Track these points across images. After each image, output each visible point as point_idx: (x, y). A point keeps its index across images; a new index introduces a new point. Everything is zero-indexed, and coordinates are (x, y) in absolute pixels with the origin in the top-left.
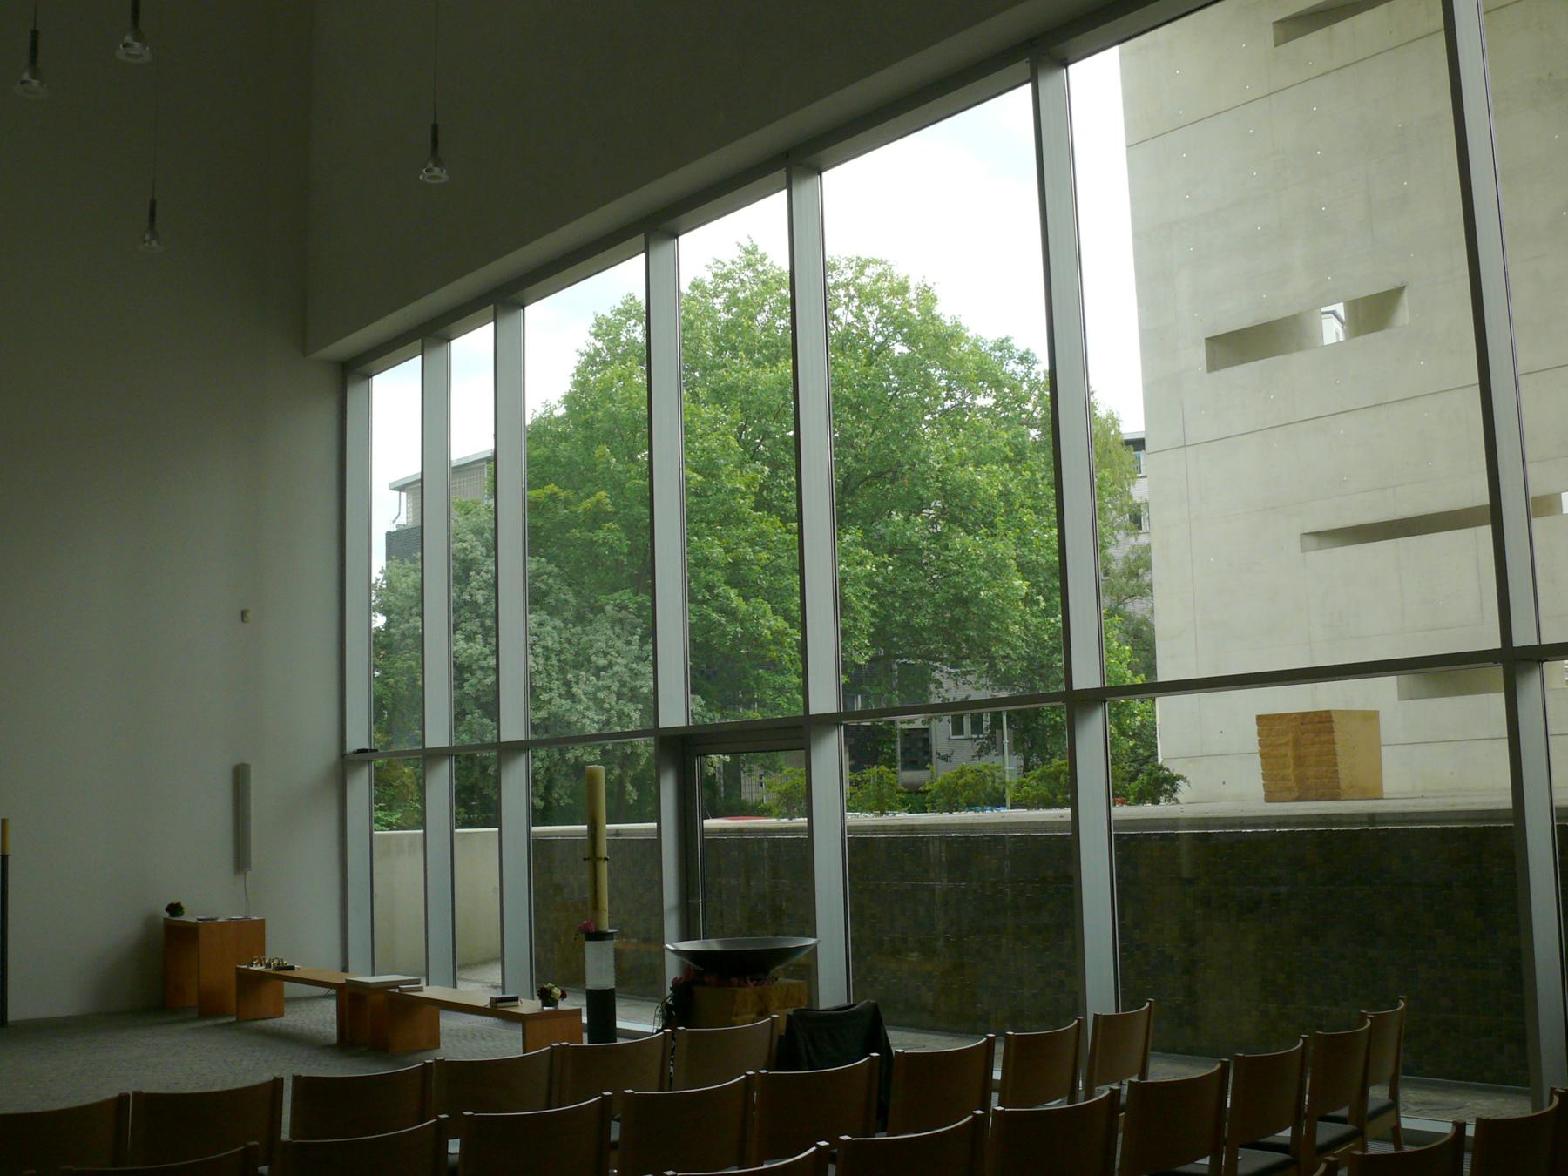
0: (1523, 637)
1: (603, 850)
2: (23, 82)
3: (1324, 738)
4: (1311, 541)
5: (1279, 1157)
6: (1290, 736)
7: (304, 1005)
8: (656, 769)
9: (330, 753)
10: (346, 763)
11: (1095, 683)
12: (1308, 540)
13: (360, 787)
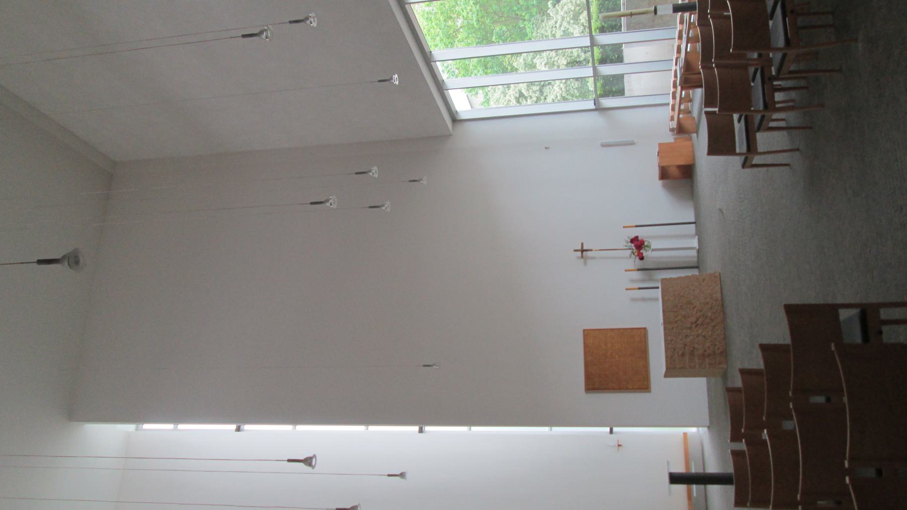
1: (629, 11)
2: (386, 209)
5: (769, 9)
7: (709, 503)
8: (593, 36)
9: (596, 113)
10: (599, 109)
13: (607, 102)
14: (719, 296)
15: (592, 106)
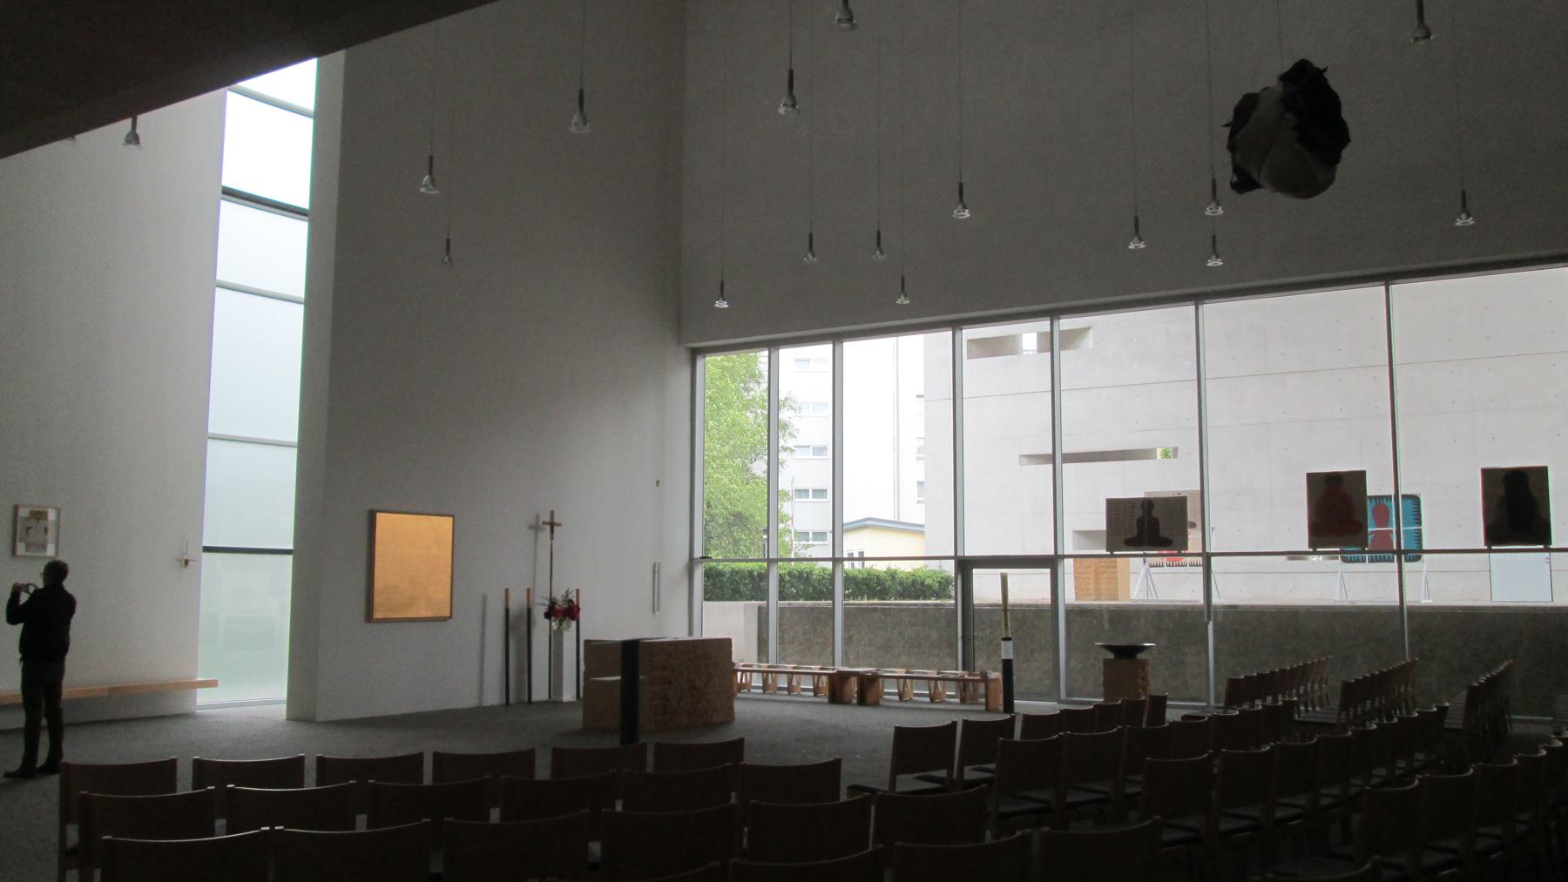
0: (1059, 553)
3: (1112, 570)
4: (1025, 460)
6: (1093, 569)
10: (692, 563)
11: (776, 557)
12: (1023, 459)
15: (698, 553)
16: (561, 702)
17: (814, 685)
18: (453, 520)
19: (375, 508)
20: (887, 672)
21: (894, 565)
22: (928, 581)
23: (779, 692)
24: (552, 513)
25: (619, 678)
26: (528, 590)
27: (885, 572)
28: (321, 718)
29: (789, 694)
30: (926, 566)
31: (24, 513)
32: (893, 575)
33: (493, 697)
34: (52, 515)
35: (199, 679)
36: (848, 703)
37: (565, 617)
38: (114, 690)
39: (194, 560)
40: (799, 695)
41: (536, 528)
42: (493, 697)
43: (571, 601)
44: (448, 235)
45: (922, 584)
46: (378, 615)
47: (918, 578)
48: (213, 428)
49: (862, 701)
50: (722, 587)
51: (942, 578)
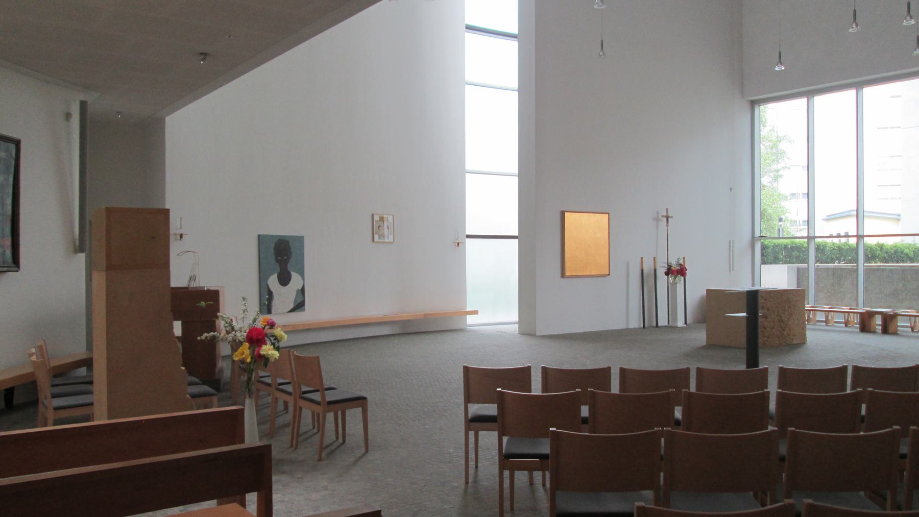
9: (749, 235)
10: (753, 239)
14: (795, 342)
15: (757, 234)
16: (677, 327)
17: (845, 319)
18: (609, 216)
19: (565, 210)
20: (900, 311)
21: (882, 240)
22: (906, 251)
23: (818, 323)
24: (667, 210)
25: (744, 314)
26: (654, 258)
27: (875, 245)
28: (538, 334)
29: (826, 325)
30: (902, 241)
31: (377, 218)
32: (881, 247)
33: (635, 322)
34: (390, 218)
35: (467, 310)
36: (874, 332)
37: (678, 274)
38: (425, 315)
39: (186, 234)
40: (833, 326)
41: (657, 219)
42: (635, 322)
43: (681, 265)
44: (602, 38)
45: (902, 252)
46: (567, 274)
47: (899, 249)
48: (468, 167)
49: (885, 331)
50: (771, 256)
51: (916, 248)
